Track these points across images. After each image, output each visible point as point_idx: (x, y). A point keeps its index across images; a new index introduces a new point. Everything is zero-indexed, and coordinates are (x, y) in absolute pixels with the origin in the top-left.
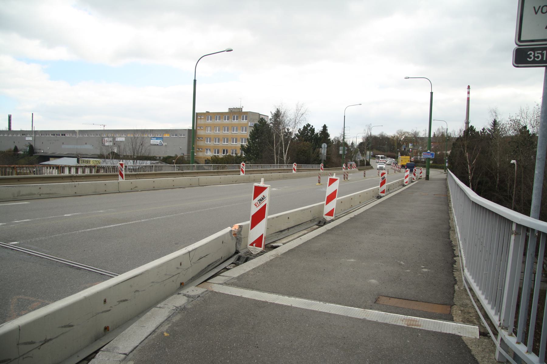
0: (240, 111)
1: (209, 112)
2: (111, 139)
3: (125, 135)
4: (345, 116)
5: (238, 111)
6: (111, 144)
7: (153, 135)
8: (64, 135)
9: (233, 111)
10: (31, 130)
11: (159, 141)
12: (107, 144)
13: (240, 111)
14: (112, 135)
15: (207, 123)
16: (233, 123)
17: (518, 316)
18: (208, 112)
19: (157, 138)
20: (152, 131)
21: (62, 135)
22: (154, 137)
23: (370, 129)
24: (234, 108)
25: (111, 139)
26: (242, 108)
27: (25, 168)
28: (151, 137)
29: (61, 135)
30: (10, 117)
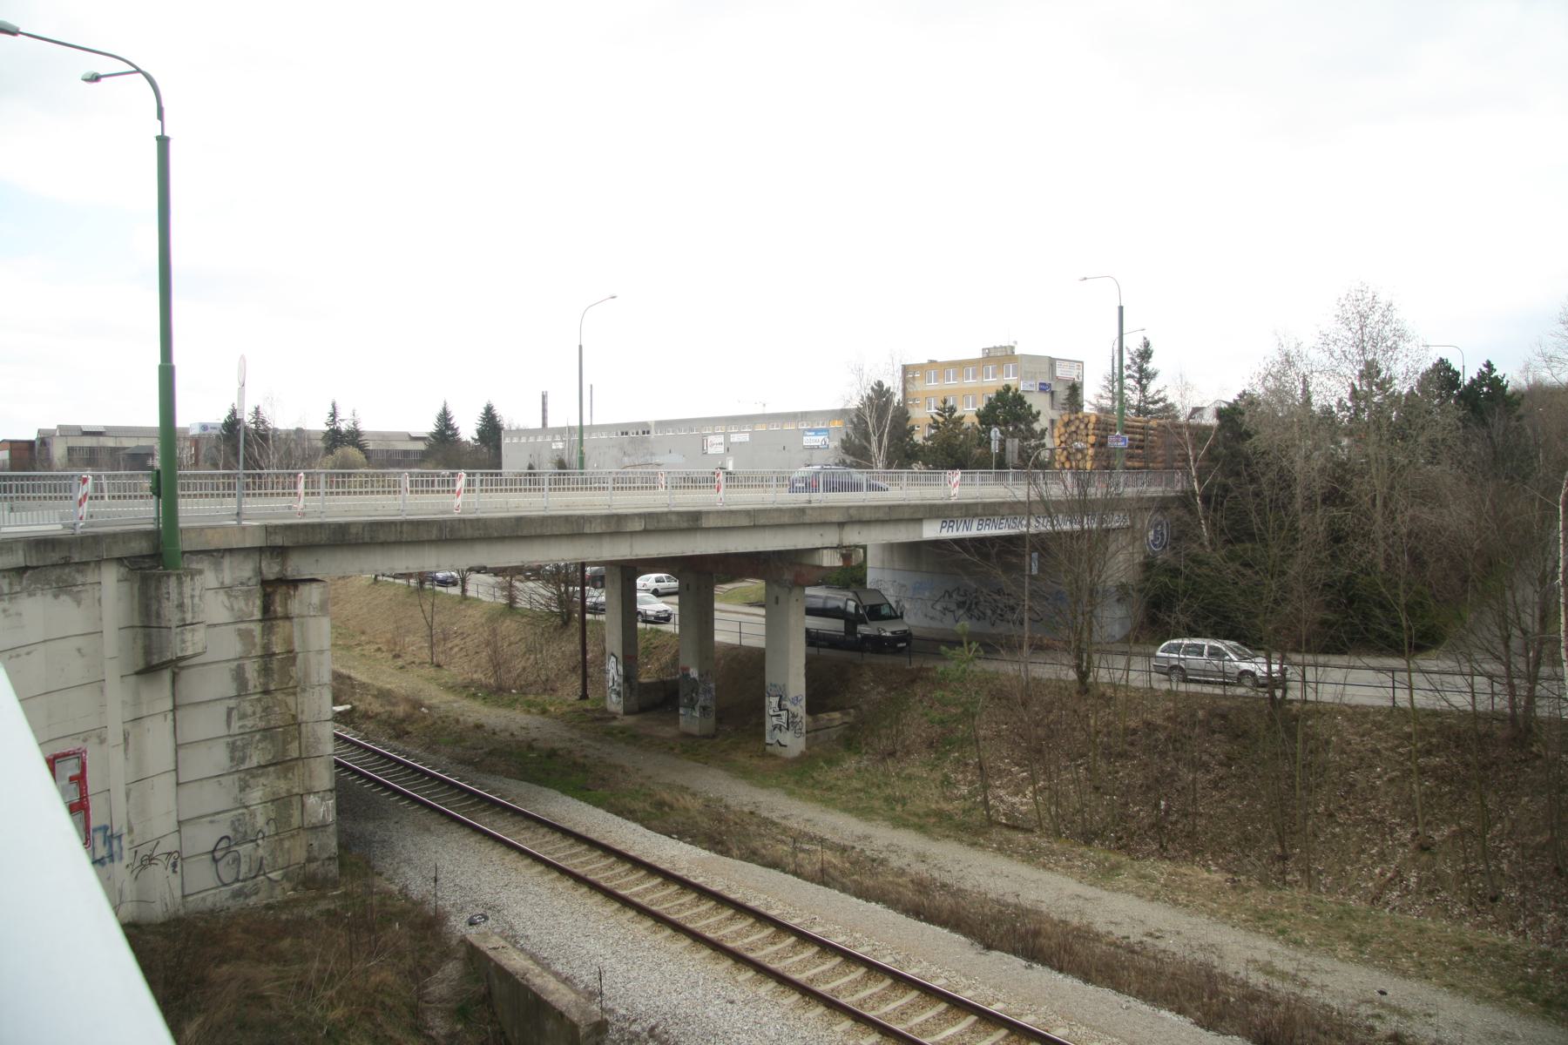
0: (1009, 353)
1: (935, 362)
2: (721, 439)
3: (749, 427)
4: (581, 347)
5: (1004, 354)
6: (721, 450)
7: (823, 424)
8: (627, 434)
9: (992, 354)
10: (537, 424)
11: (821, 438)
12: (711, 451)
13: (1009, 353)
14: (724, 427)
15: (927, 388)
16: (984, 385)
17: (92, 537)
18: (932, 362)
19: (817, 432)
20: (804, 416)
21: (622, 434)
22: (810, 430)
23: (860, 371)
24: (995, 348)
25: (721, 439)
26: (1012, 344)
27: (1485, 680)
28: (805, 430)
29: (640, 432)
30: (544, 397)
